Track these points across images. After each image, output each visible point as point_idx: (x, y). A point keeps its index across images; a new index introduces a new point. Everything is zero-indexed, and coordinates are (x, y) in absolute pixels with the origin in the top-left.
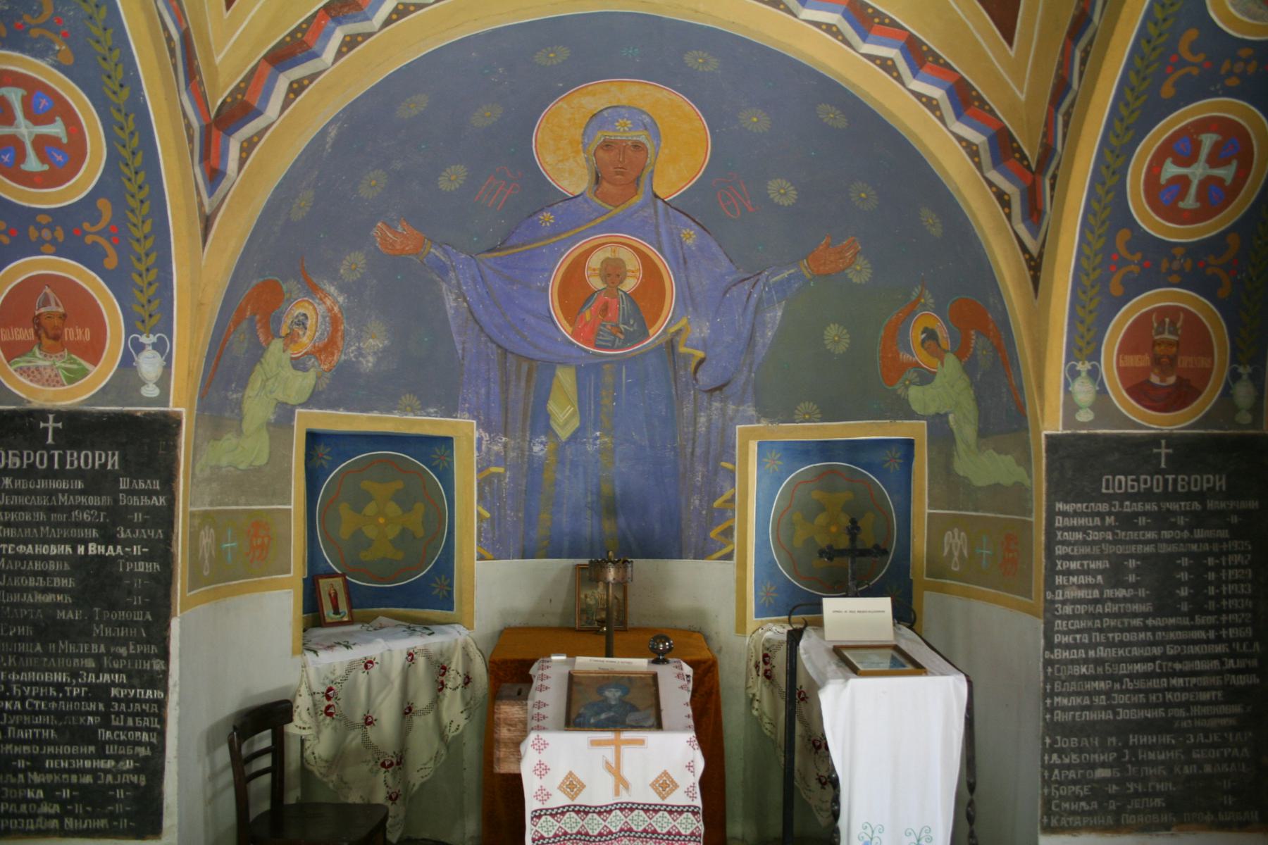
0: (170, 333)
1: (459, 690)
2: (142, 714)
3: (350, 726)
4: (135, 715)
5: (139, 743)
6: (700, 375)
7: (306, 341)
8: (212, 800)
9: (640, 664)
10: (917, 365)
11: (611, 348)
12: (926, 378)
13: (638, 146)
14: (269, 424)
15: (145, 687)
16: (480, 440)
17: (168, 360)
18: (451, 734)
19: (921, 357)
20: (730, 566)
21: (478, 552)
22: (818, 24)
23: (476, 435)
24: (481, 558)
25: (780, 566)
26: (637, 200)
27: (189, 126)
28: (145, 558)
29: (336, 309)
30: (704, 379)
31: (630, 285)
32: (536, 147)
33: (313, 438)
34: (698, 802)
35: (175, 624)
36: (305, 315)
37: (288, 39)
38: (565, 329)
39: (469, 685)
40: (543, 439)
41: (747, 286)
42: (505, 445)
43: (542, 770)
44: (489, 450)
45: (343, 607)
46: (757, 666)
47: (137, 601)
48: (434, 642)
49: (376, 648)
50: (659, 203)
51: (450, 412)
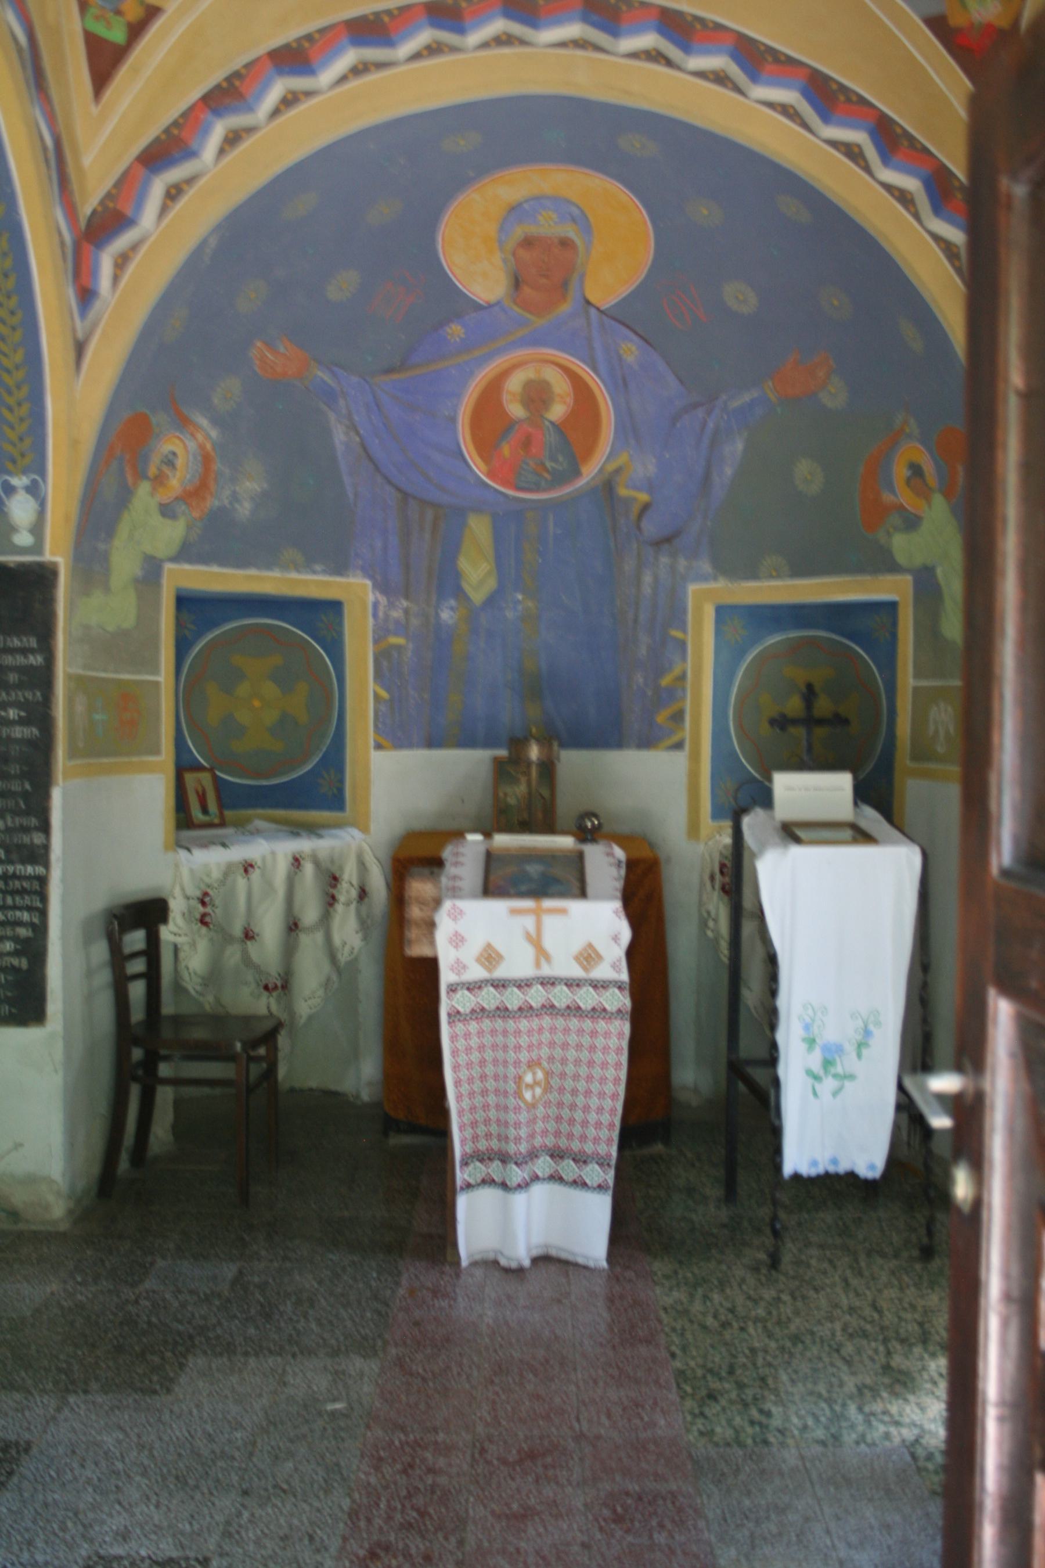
0: (42, 471)
1: (353, 907)
2: (23, 892)
3: (227, 938)
4: (14, 893)
5: (19, 923)
6: (645, 524)
7: (176, 483)
8: (89, 998)
9: (566, 842)
10: (901, 508)
11: (537, 489)
12: (912, 523)
13: (566, 243)
14: (136, 581)
15: (23, 862)
16: (376, 605)
17: (42, 504)
18: (343, 957)
19: (905, 497)
20: (680, 760)
21: (375, 741)
22: (771, 105)
23: (371, 598)
24: (379, 747)
25: (743, 761)
26: (565, 308)
27: (62, 244)
28: (22, 722)
29: (209, 446)
30: (650, 528)
31: (557, 412)
32: (443, 247)
33: (184, 602)
34: (624, 976)
35: (57, 795)
36: (174, 454)
37: (163, 137)
38: (478, 468)
39: (366, 900)
40: (453, 602)
41: (700, 413)
42: (406, 612)
43: (458, 940)
44: (387, 616)
45: (212, 806)
46: (712, 878)
47: (14, 769)
48: (323, 845)
49: (256, 849)
50: (593, 312)
51: (340, 568)
